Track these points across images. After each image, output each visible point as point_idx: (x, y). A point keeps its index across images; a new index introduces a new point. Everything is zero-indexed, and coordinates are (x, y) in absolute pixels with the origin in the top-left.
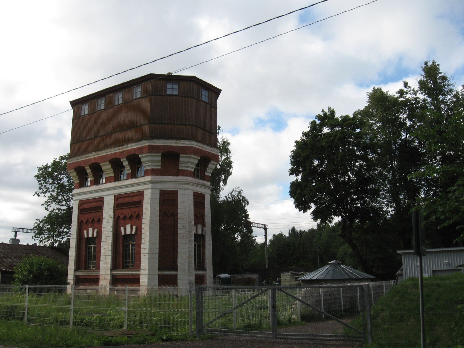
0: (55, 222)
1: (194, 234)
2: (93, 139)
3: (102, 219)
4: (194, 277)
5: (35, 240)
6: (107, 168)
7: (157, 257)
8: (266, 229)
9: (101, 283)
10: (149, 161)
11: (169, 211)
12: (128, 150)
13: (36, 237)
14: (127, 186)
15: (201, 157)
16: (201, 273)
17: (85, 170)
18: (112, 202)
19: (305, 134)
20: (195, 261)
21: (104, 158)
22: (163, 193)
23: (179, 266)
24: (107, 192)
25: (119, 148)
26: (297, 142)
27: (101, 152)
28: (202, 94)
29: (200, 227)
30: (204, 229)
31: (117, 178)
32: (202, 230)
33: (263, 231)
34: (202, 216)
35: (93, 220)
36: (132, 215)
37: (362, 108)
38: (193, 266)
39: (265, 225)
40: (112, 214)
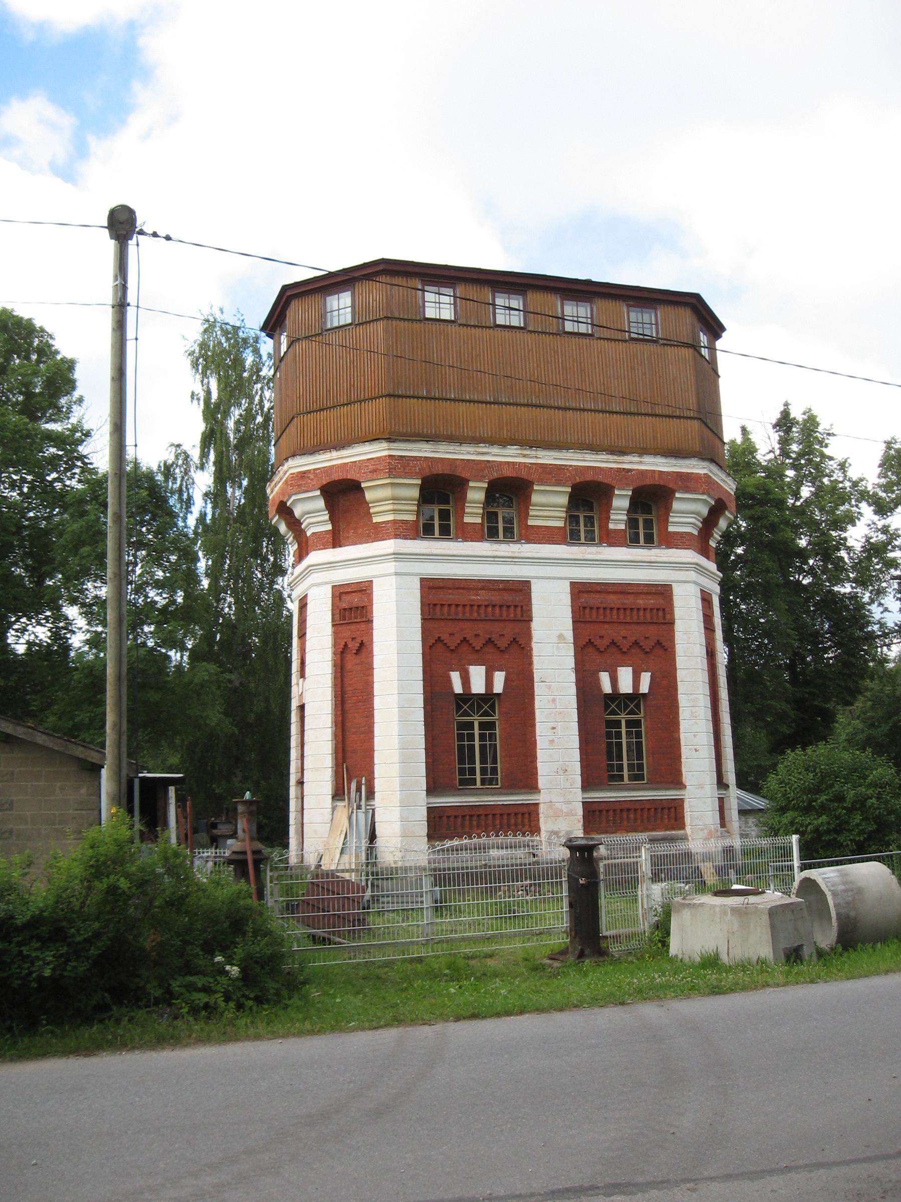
10: (386, 500)
21: (553, 474)
22: (340, 592)
25: (611, 457)
37: (57, 344)
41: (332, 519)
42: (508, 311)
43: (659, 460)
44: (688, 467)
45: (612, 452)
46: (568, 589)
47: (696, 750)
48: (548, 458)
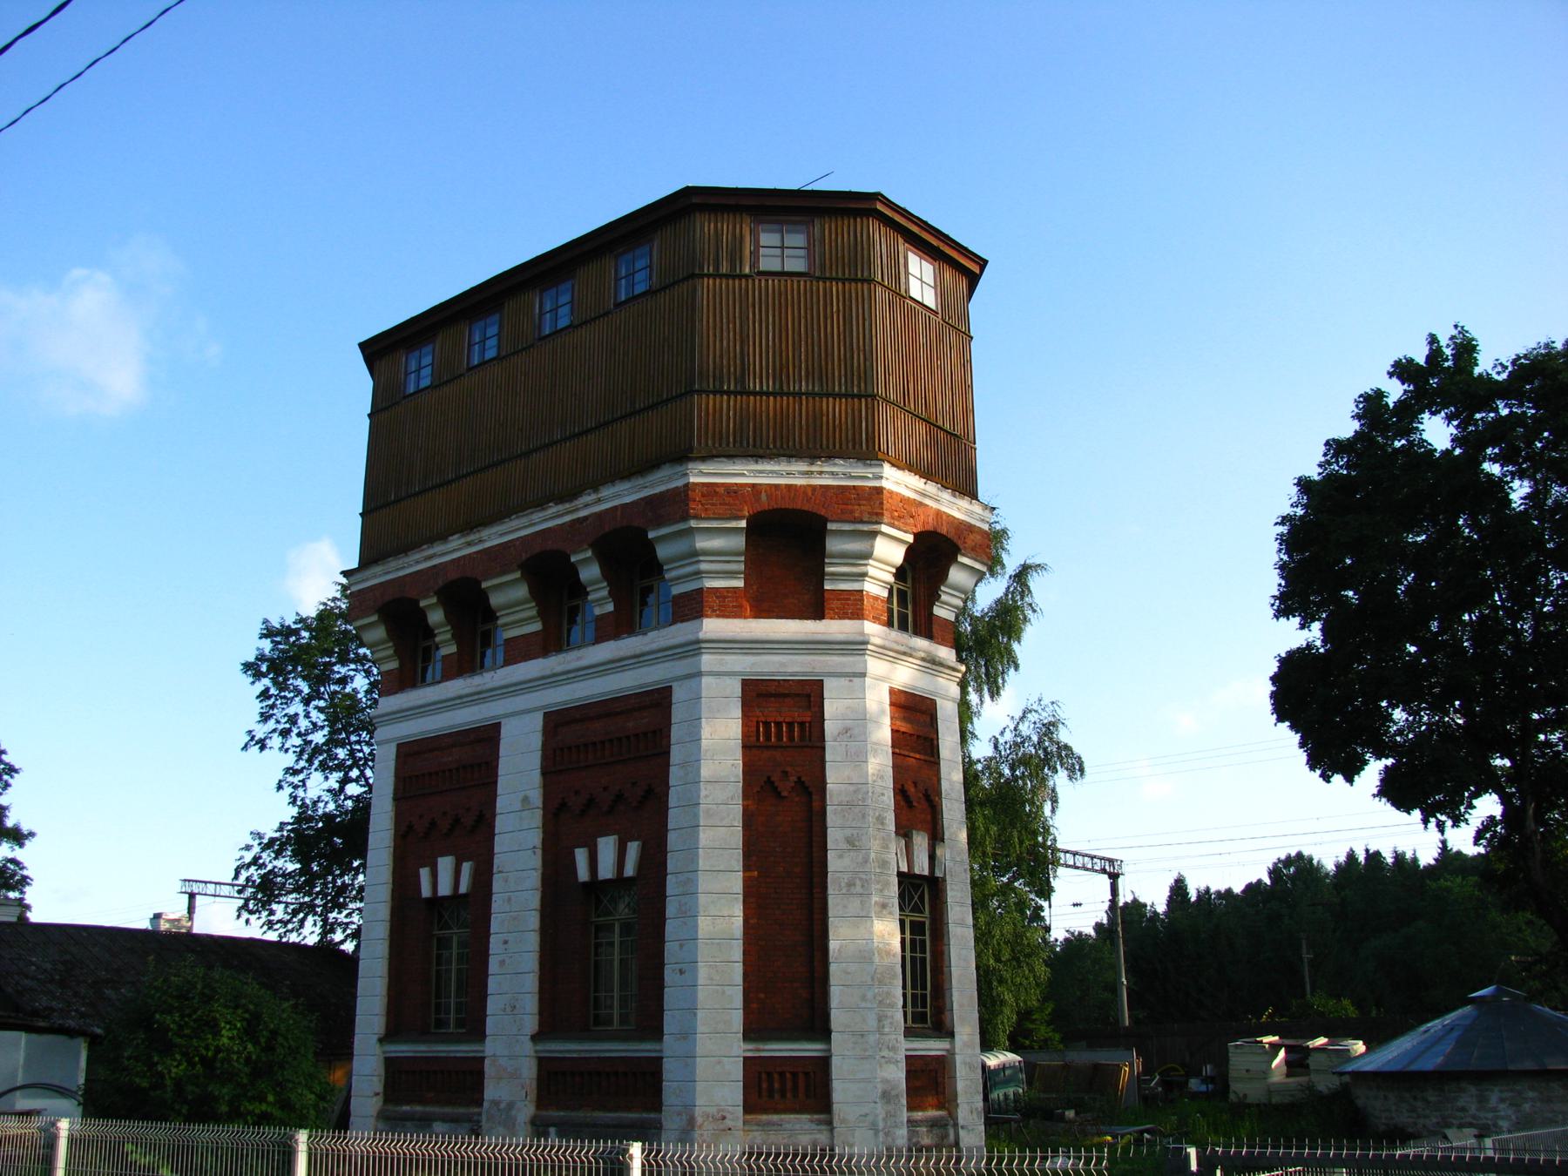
0: (318, 848)
1: (900, 874)
2: (449, 482)
3: (494, 815)
4: (903, 1065)
5: (247, 921)
6: (510, 597)
7: (737, 972)
8: (1114, 877)
9: (490, 1092)
11: (785, 773)
12: (599, 515)
13: (251, 912)
14: (597, 671)
15: (916, 536)
16: (933, 1047)
17: (422, 615)
18: (537, 741)
19: (1336, 447)
20: (904, 995)
21: (497, 559)
23: (837, 1018)
24: (516, 704)
26: (1304, 484)
27: (485, 533)
28: (907, 273)
29: (921, 841)
30: (939, 852)
31: (551, 641)
32: (932, 857)
33: (1105, 881)
34: (927, 797)
35: (457, 821)
36: (619, 797)
38: (899, 1016)
39: (1111, 861)
40: (536, 797)
41: (542, 615)
42: (486, 340)
43: (621, 487)
44: (662, 482)
45: (560, 500)
46: (737, 690)
47: (681, 972)
48: (493, 537)
